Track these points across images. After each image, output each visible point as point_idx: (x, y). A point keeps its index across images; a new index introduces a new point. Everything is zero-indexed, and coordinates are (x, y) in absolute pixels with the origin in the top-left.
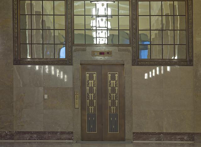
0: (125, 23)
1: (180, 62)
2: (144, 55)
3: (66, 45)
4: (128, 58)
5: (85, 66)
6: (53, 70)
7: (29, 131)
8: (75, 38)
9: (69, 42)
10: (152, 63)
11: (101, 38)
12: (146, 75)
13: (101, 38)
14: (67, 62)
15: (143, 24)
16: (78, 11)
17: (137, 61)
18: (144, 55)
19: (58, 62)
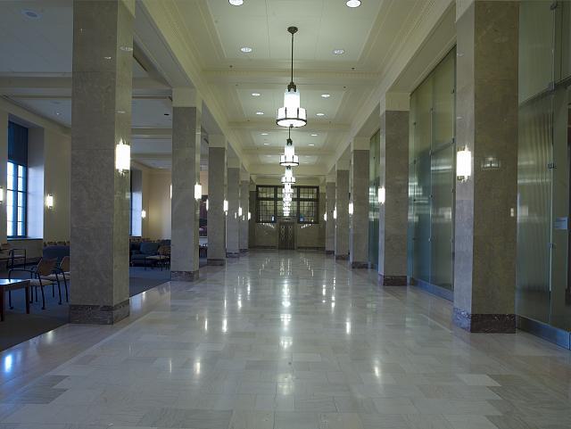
0: (295, 209)
1: (315, 223)
2: (302, 220)
3: (407, 200)
4: (296, 221)
5: (281, 224)
6: (269, 225)
7: (211, 110)
8: (277, 214)
9: (275, 216)
10: (305, 223)
11: (286, 214)
12: (249, 217)
13: (286, 214)
14: (275, 222)
15: (301, 209)
16: (407, 121)
17: (299, 222)
18: (302, 220)
19: (272, 222)
